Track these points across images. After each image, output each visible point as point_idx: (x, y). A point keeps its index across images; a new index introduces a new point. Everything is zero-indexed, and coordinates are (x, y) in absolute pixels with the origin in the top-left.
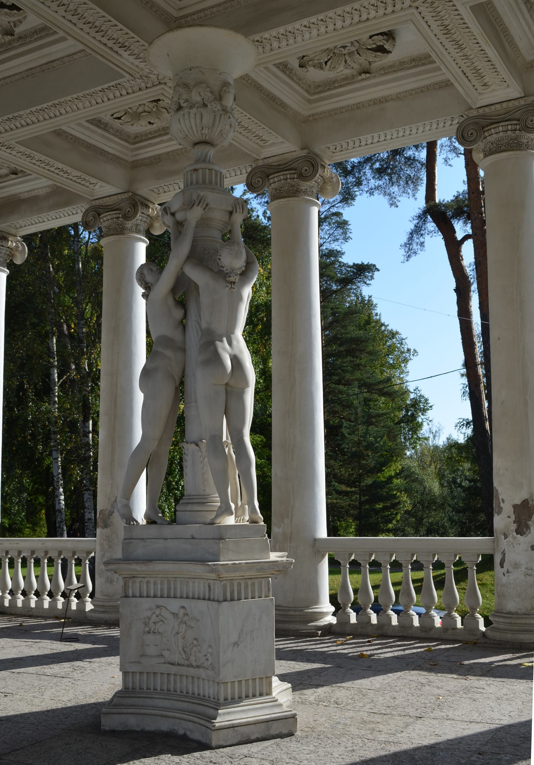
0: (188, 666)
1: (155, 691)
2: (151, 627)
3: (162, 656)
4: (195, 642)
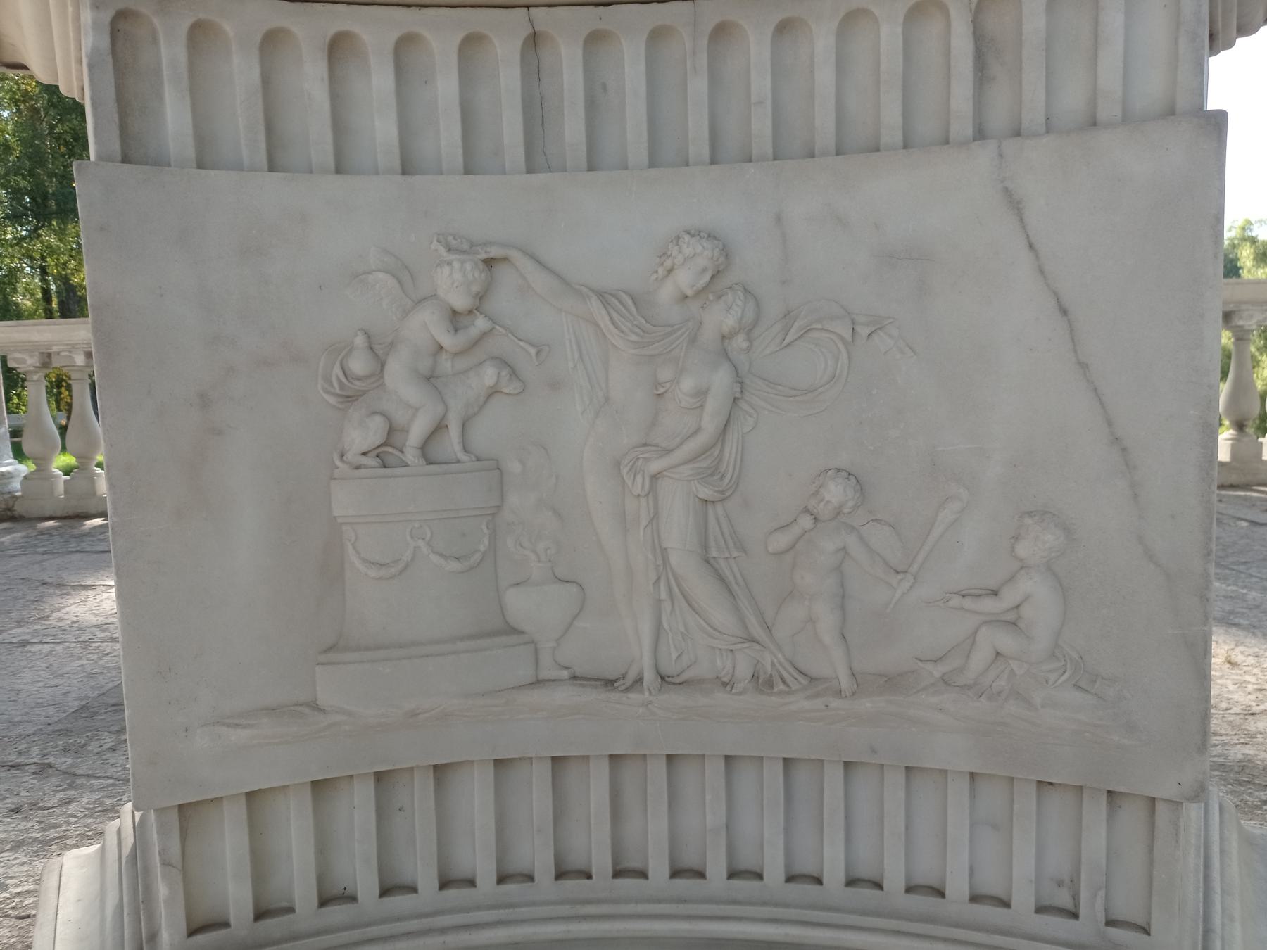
0: (763, 683)
1: (454, 895)
2: (400, 417)
3: (513, 631)
4: (835, 492)
